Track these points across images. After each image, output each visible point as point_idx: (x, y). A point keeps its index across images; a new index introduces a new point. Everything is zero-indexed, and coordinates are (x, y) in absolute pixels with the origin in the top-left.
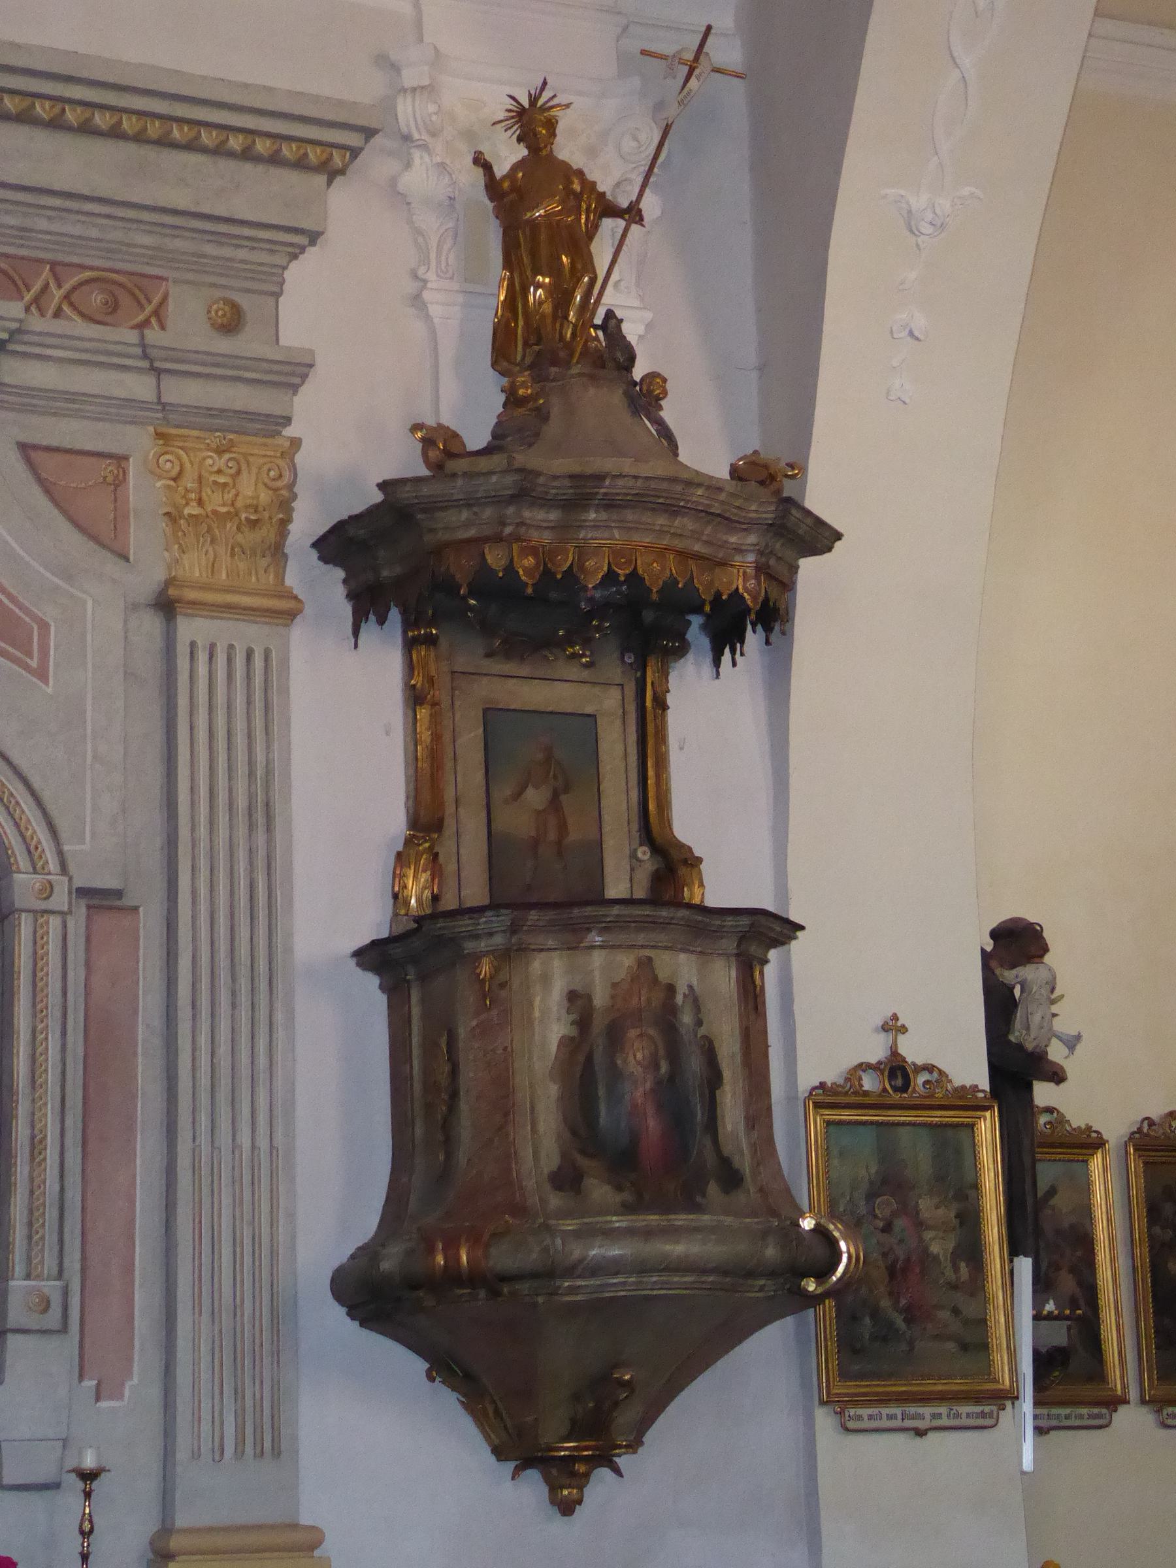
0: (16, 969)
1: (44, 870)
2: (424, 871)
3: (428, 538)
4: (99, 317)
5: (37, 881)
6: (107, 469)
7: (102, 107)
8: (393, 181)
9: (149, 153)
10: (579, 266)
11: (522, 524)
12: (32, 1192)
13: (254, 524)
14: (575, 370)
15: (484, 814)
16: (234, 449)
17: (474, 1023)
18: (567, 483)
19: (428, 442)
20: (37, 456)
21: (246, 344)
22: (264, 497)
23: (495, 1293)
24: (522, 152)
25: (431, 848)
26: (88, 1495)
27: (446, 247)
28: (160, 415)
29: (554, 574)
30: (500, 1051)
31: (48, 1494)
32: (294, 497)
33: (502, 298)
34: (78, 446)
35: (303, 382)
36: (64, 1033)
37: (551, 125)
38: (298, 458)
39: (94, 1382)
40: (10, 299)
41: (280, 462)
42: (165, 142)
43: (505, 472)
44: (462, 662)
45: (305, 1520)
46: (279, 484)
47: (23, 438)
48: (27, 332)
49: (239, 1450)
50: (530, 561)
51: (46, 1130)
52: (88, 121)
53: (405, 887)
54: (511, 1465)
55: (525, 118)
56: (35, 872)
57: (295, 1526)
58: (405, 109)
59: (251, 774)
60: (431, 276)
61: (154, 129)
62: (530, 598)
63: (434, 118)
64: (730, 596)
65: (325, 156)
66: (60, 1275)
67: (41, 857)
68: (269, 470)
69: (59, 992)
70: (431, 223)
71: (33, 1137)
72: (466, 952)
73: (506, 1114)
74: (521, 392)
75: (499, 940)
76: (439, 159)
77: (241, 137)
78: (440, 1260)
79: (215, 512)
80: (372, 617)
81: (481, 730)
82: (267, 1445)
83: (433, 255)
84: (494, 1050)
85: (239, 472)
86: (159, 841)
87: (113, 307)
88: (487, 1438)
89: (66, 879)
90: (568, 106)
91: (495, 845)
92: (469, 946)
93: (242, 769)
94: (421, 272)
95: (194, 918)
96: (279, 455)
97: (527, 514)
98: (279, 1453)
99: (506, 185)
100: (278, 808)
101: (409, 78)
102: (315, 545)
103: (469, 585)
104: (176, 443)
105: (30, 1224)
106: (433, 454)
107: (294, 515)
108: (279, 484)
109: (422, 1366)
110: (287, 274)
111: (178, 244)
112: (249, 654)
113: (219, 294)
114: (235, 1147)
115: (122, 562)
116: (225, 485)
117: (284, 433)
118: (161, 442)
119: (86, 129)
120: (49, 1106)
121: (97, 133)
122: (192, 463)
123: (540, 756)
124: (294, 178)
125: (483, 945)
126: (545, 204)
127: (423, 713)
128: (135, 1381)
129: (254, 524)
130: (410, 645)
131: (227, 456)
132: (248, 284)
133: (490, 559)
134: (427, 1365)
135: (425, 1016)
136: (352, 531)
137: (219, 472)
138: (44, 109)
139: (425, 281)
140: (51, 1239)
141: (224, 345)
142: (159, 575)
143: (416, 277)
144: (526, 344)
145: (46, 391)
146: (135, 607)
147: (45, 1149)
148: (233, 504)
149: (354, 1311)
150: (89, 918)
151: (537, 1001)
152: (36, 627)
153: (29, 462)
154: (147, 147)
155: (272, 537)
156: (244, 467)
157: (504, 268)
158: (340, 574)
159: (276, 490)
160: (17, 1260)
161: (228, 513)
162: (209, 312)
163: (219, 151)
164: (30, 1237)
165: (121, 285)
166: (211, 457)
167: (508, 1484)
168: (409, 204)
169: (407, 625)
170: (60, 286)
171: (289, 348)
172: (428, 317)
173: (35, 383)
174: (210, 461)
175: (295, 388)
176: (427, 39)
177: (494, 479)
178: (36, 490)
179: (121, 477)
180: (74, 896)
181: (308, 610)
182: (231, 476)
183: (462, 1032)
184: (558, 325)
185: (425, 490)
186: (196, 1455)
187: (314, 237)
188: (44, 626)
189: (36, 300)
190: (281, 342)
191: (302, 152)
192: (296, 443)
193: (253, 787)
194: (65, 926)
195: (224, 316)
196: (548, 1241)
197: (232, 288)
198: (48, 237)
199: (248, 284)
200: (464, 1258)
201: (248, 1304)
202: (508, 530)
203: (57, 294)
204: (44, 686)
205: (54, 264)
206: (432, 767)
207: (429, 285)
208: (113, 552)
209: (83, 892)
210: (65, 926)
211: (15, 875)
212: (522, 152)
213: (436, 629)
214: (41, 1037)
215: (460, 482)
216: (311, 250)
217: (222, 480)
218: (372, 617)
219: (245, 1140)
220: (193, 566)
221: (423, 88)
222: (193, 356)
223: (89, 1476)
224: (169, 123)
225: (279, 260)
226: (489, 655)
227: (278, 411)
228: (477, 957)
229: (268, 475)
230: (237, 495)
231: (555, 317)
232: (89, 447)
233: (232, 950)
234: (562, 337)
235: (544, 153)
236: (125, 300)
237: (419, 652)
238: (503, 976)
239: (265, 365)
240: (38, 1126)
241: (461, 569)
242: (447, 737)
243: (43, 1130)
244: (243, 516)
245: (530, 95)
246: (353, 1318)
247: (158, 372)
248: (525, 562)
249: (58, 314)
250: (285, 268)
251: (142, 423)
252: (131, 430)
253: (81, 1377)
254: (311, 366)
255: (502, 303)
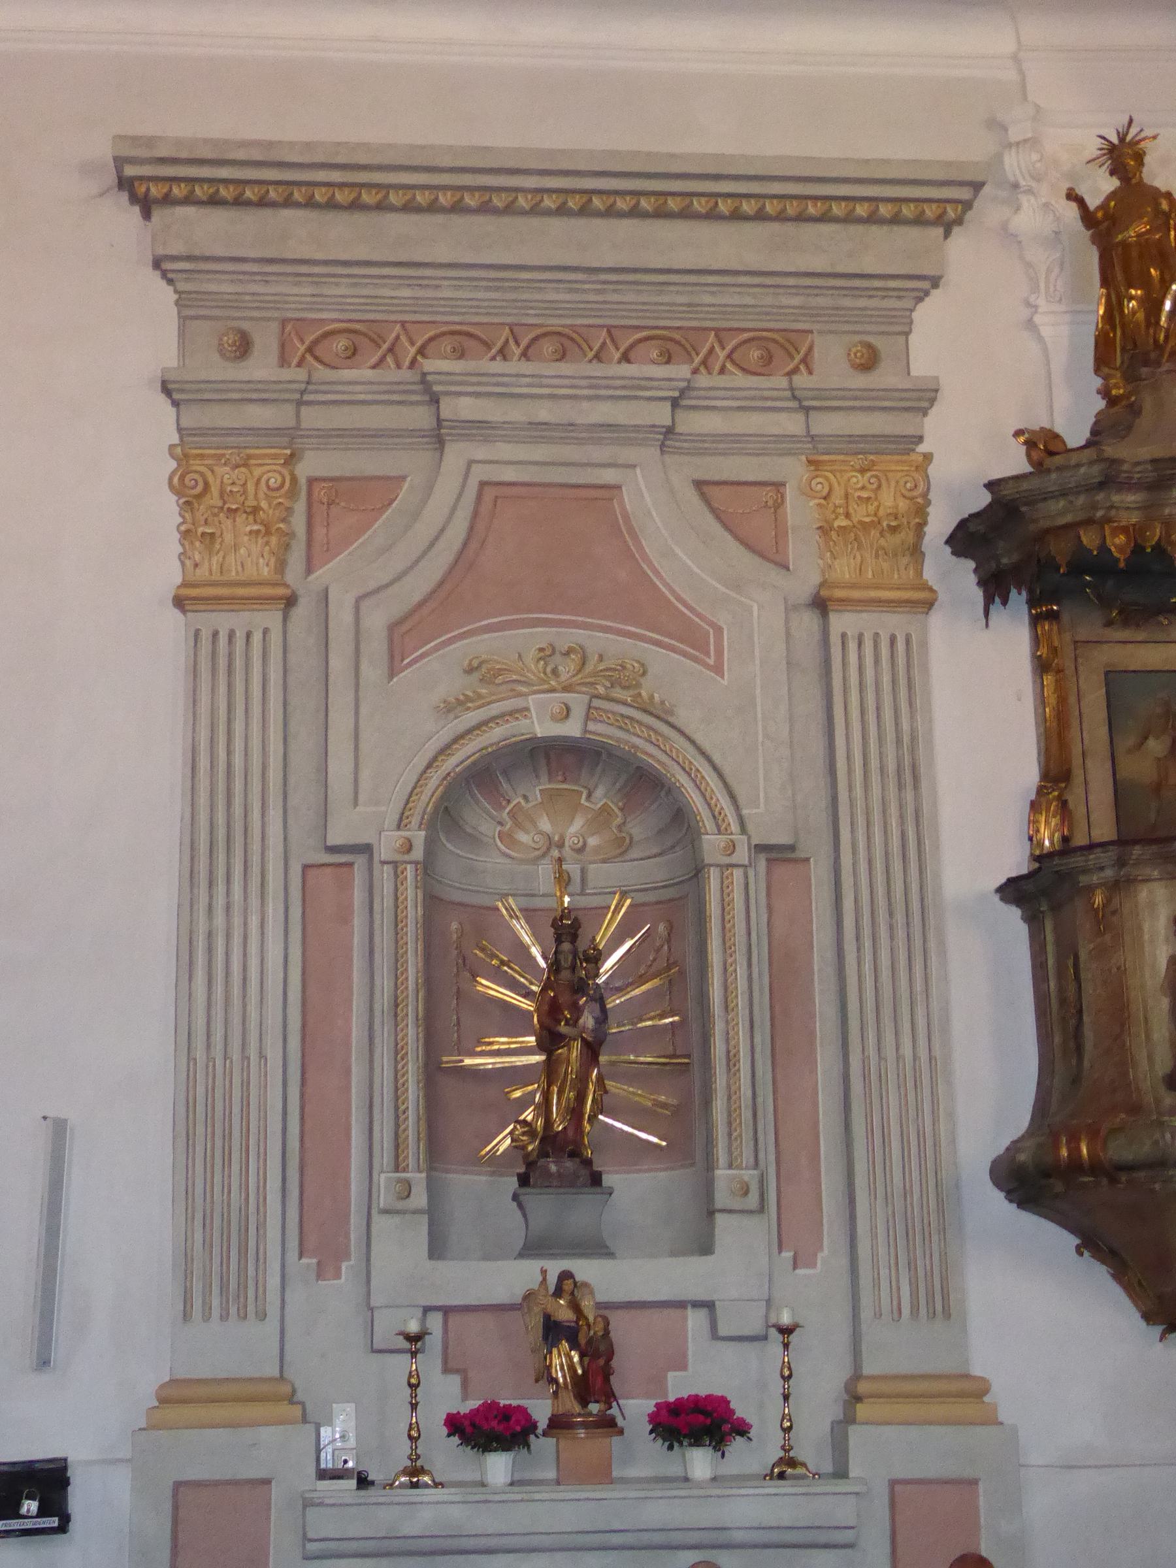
0: (708, 914)
1: (727, 831)
2: (1054, 816)
3: (1032, 527)
4: (759, 370)
5: (721, 840)
6: (768, 495)
7: (748, 196)
8: (1004, 226)
9: (790, 228)
10: (1167, 277)
11: (1112, 507)
12: (729, 1098)
13: (894, 530)
14: (1164, 368)
15: (1109, 764)
16: (875, 468)
17: (1092, 946)
18: (1149, 467)
19: (1030, 444)
20: (713, 492)
21: (885, 377)
22: (903, 505)
23: (1113, 1180)
24: (1113, 184)
25: (1059, 797)
26: (786, 1346)
27: (1053, 276)
28: (810, 446)
29: (1144, 548)
30: (1114, 970)
31: (757, 1345)
32: (929, 503)
33: (1101, 312)
34: (744, 479)
35: (932, 406)
36: (750, 965)
37: (1139, 157)
38: (932, 470)
39: (792, 1254)
40: (684, 363)
41: (916, 475)
42: (801, 218)
43: (1091, 463)
44: (1083, 633)
45: (977, 1371)
46: (915, 493)
47: (701, 475)
48: (695, 389)
49: (931, 1311)
50: (1121, 539)
51: (739, 1045)
52: (736, 209)
53: (1038, 831)
54: (1158, 1330)
55: (1116, 152)
56: (720, 833)
57: (967, 1377)
58: (1013, 164)
59: (899, 741)
60: (1041, 302)
61: (792, 209)
62: (1122, 571)
63: (1038, 165)
64: (1153, 548)
65: (940, 211)
66: (756, 1164)
67: (724, 820)
68: (906, 483)
69: (744, 932)
70: (1042, 258)
71: (728, 1052)
72: (1081, 885)
73: (1123, 1025)
74: (1114, 392)
75: (1109, 873)
76: (1044, 200)
77: (866, 205)
78: (1064, 1153)
79: (861, 522)
80: (997, 599)
81: (1104, 690)
82: (939, 1307)
83: (1042, 285)
84: (1110, 970)
85: (879, 486)
86: (824, 803)
87: (768, 359)
88: (1136, 1305)
89: (745, 837)
90: (1155, 137)
91: (1121, 792)
92: (1084, 880)
93: (890, 736)
94: (1032, 299)
95: (855, 864)
96: (913, 469)
97: (1116, 498)
98: (950, 1315)
99: (1100, 215)
100: (922, 770)
101: (1014, 135)
102: (947, 542)
103: (1069, 564)
104: (825, 468)
105: (730, 1124)
106: (1035, 455)
107: (929, 518)
108: (915, 493)
109: (1074, 1241)
110: (915, 315)
111: (821, 301)
112: (893, 640)
113: (857, 338)
114: (899, 1057)
115: (784, 572)
116: (869, 499)
117: (917, 450)
118: (812, 468)
119: (736, 216)
120: (740, 1025)
121: (746, 218)
122: (839, 483)
123: (1159, 710)
124: (914, 232)
125: (1095, 879)
126: (1134, 225)
127: (1049, 679)
128: (826, 1251)
129: (894, 530)
130: (1035, 621)
131: (869, 474)
132: (883, 328)
133: (1085, 540)
134: (1077, 1241)
135: (1058, 943)
136: (972, 527)
137: (863, 488)
138: (700, 203)
139: (1036, 307)
140: (747, 1135)
141: (861, 381)
142: (815, 579)
143: (1028, 304)
144: (1123, 349)
145: (714, 436)
146: (796, 608)
147: (739, 1061)
148: (876, 515)
149: (1011, 1195)
150: (769, 872)
151: (1146, 927)
152: (711, 631)
153: (704, 497)
154: (789, 224)
155: (911, 539)
156: (884, 482)
157: (1102, 286)
158: (971, 564)
159: (912, 499)
160: (720, 1153)
161: (873, 521)
162: (849, 354)
163: (849, 219)
164: (730, 1135)
165: (774, 341)
166: (856, 477)
167: (1159, 1346)
168: (1020, 242)
169: (1032, 603)
170: (723, 348)
171: (917, 377)
172: (1040, 339)
173: (705, 431)
174: (854, 480)
175: (925, 412)
176: (1030, 98)
177: (1083, 470)
178: (710, 518)
179: (779, 501)
180: (753, 851)
181: (942, 596)
182: (872, 490)
183: (1083, 955)
184: (1151, 331)
185: (1025, 486)
186: (878, 1315)
187: (935, 282)
188: (719, 630)
189: (704, 363)
190: (913, 373)
191: (920, 208)
192: (928, 457)
193: (900, 752)
194: (746, 877)
195: (862, 356)
196: (1157, 1136)
197: (869, 333)
198: (712, 309)
199: (883, 328)
200: (1085, 1151)
201: (916, 1188)
202: (1100, 514)
203: (722, 355)
204: (719, 679)
205: (717, 331)
206: (1058, 725)
207: (1040, 310)
208: (776, 563)
209: (761, 848)
210: (746, 877)
211: (705, 837)
212: (1113, 184)
213: (1056, 605)
214: (731, 969)
215: (1054, 476)
216: (934, 292)
217: (865, 494)
218: (997, 599)
219: (907, 1051)
220: (844, 569)
221: (1025, 141)
222: (834, 393)
223: (787, 1331)
224: (804, 202)
225: (907, 304)
226: (1109, 623)
227: (910, 431)
228: (1090, 889)
229: (905, 486)
230: (878, 507)
231: (1148, 325)
232: (751, 478)
233: (889, 892)
234: (1156, 341)
235: (1134, 181)
236: (778, 352)
237: (1043, 627)
238: (1116, 902)
239: (897, 394)
240: (732, 1043)
241: (1061, 550)
242: (1072, 700)
243: (737, 1046)
244: (885, 524)
245: (1118, 133)
246: (1011, 1201)
247: (807, 410)
248: (1117, 541)
249: (722, 371)
250: (912, 311)
251: (795, 454)
252: (789, 461)
253: (780, 1251)
254: (937, 391)
255: (1103, 317)
